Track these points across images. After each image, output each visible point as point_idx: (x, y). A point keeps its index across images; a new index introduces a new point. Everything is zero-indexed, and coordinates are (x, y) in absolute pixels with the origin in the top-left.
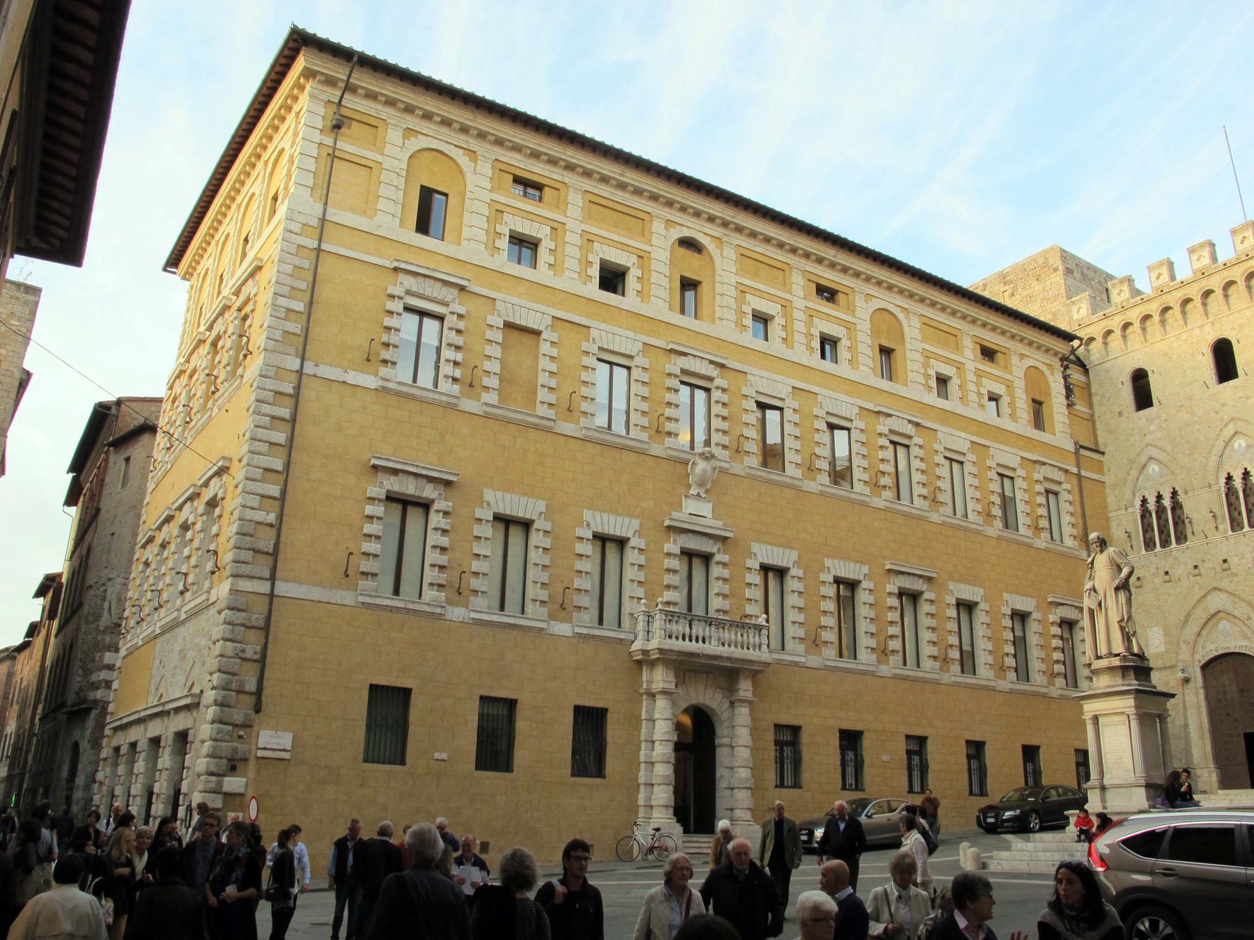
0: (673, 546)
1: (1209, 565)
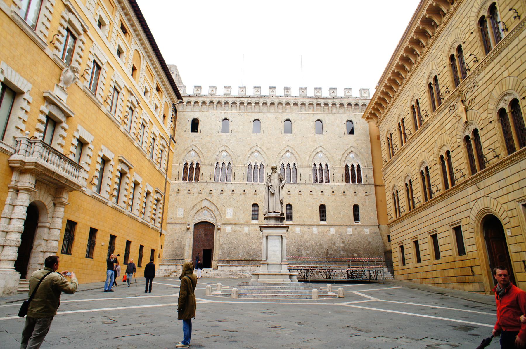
0: (46, 109)
1: (205, 190)
